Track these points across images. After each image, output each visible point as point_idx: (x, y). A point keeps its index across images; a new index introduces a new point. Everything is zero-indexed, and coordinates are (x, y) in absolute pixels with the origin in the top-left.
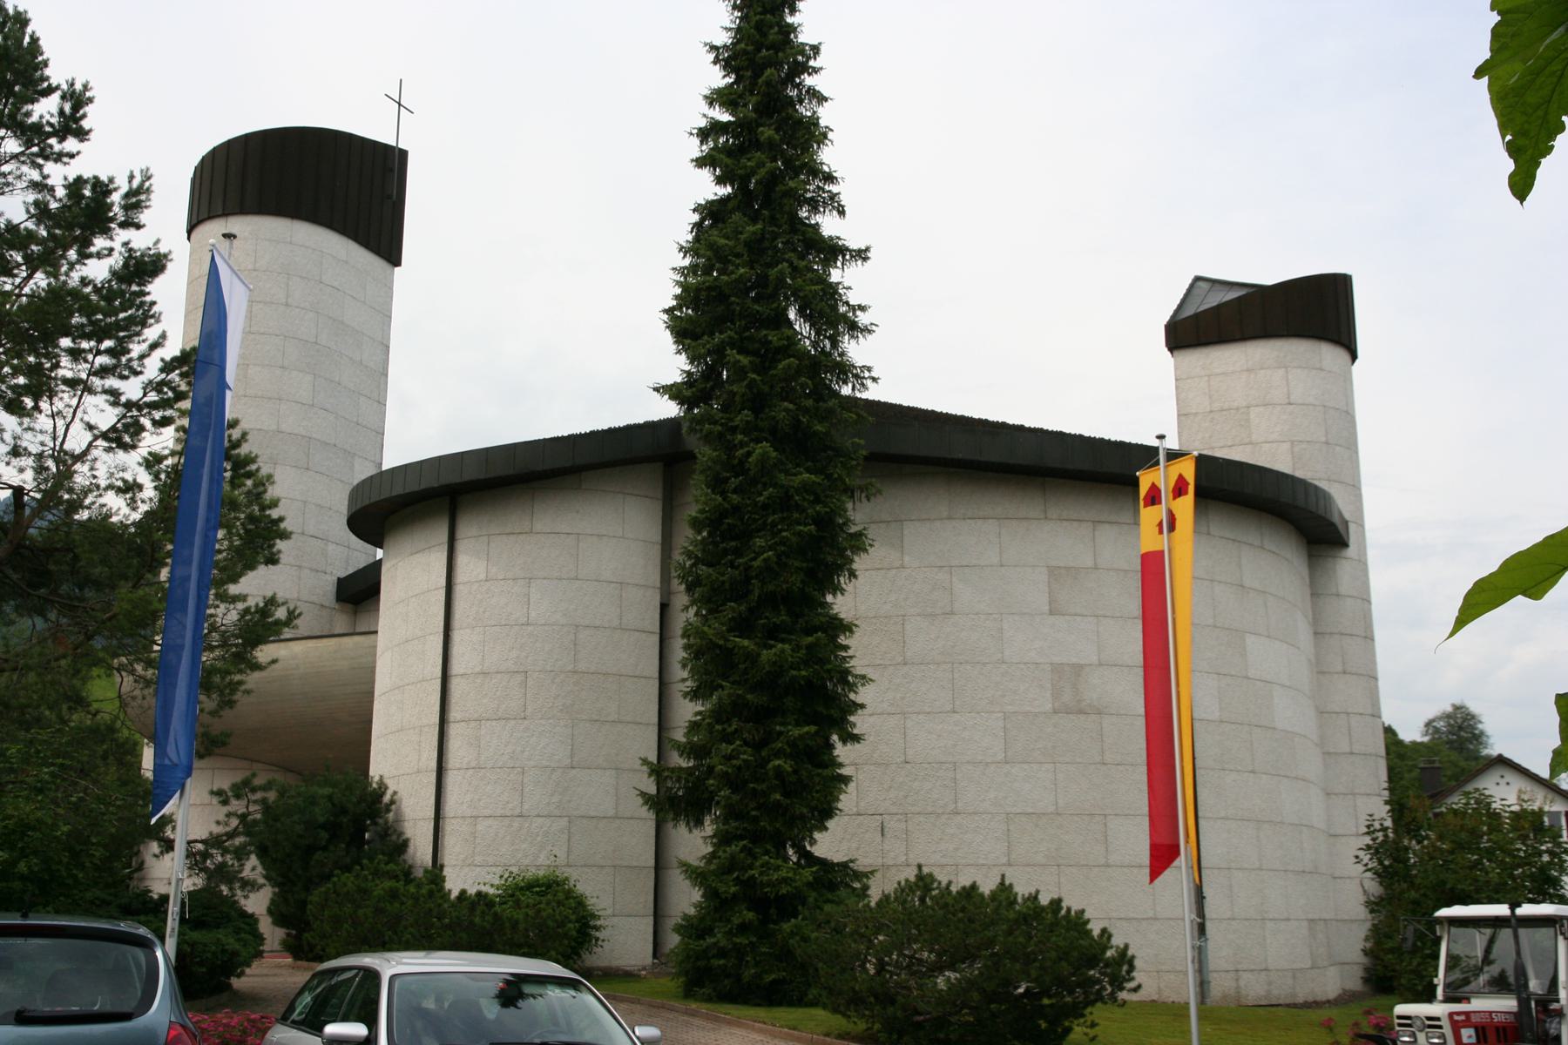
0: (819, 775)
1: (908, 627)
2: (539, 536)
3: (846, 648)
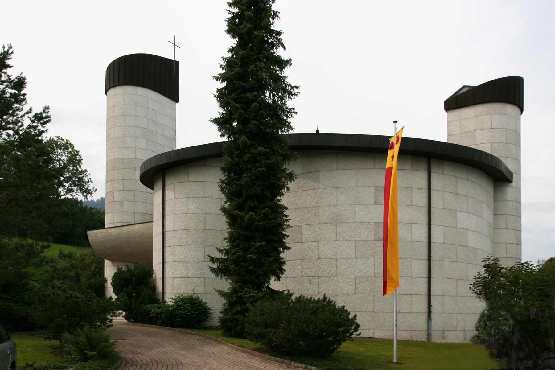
0: (268, 260)
1: (320, 210)
2: (191, 183)
3: (287, 216)
